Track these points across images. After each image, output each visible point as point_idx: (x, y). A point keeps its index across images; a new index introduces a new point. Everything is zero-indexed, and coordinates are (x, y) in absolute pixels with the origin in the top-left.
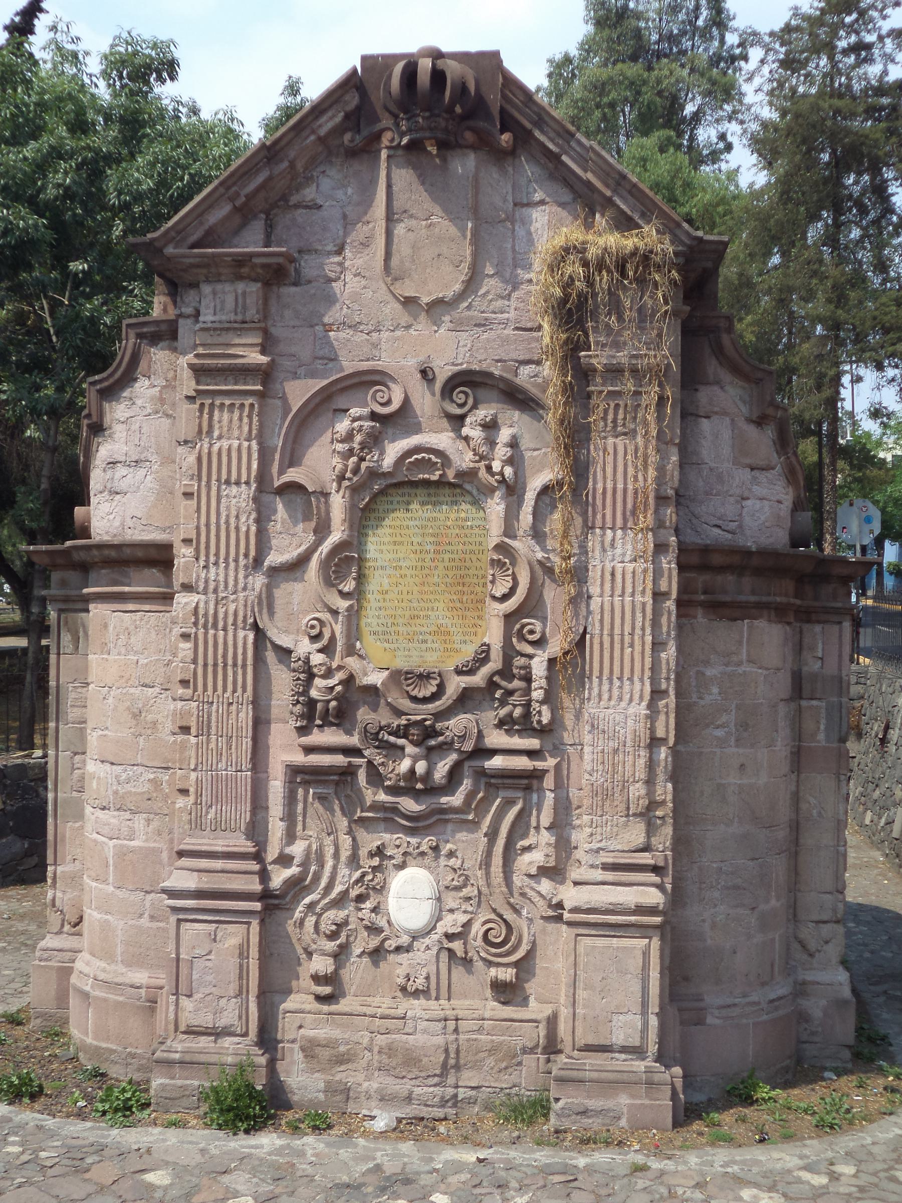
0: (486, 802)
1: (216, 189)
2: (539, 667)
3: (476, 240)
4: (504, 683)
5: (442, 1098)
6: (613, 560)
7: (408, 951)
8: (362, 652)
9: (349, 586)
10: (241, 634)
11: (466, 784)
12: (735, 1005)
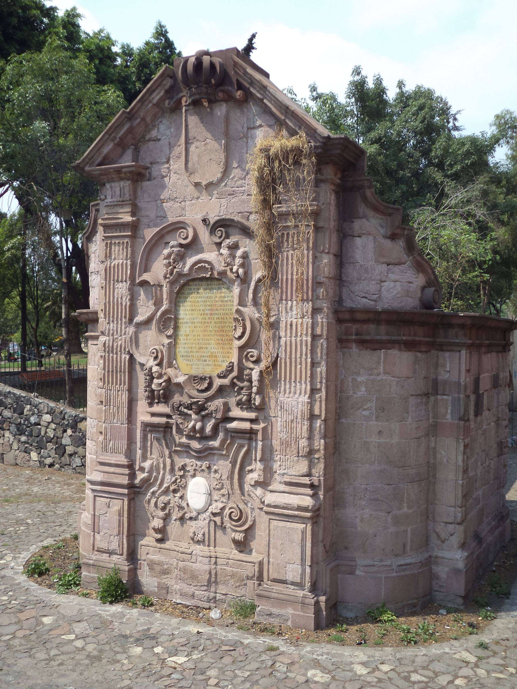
0: (231, 444)
1: (103, 136)
2: (255, 376)
3: (227, 149)
4: (238, 383)
5: (208, 597)
6: (292, 317)
7: (196, 520)
8: (176, 366)
9: (170, 332)
10: (123, 356)
11: (221, 435)
12: (373, 565)
